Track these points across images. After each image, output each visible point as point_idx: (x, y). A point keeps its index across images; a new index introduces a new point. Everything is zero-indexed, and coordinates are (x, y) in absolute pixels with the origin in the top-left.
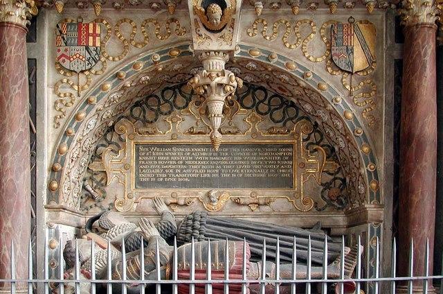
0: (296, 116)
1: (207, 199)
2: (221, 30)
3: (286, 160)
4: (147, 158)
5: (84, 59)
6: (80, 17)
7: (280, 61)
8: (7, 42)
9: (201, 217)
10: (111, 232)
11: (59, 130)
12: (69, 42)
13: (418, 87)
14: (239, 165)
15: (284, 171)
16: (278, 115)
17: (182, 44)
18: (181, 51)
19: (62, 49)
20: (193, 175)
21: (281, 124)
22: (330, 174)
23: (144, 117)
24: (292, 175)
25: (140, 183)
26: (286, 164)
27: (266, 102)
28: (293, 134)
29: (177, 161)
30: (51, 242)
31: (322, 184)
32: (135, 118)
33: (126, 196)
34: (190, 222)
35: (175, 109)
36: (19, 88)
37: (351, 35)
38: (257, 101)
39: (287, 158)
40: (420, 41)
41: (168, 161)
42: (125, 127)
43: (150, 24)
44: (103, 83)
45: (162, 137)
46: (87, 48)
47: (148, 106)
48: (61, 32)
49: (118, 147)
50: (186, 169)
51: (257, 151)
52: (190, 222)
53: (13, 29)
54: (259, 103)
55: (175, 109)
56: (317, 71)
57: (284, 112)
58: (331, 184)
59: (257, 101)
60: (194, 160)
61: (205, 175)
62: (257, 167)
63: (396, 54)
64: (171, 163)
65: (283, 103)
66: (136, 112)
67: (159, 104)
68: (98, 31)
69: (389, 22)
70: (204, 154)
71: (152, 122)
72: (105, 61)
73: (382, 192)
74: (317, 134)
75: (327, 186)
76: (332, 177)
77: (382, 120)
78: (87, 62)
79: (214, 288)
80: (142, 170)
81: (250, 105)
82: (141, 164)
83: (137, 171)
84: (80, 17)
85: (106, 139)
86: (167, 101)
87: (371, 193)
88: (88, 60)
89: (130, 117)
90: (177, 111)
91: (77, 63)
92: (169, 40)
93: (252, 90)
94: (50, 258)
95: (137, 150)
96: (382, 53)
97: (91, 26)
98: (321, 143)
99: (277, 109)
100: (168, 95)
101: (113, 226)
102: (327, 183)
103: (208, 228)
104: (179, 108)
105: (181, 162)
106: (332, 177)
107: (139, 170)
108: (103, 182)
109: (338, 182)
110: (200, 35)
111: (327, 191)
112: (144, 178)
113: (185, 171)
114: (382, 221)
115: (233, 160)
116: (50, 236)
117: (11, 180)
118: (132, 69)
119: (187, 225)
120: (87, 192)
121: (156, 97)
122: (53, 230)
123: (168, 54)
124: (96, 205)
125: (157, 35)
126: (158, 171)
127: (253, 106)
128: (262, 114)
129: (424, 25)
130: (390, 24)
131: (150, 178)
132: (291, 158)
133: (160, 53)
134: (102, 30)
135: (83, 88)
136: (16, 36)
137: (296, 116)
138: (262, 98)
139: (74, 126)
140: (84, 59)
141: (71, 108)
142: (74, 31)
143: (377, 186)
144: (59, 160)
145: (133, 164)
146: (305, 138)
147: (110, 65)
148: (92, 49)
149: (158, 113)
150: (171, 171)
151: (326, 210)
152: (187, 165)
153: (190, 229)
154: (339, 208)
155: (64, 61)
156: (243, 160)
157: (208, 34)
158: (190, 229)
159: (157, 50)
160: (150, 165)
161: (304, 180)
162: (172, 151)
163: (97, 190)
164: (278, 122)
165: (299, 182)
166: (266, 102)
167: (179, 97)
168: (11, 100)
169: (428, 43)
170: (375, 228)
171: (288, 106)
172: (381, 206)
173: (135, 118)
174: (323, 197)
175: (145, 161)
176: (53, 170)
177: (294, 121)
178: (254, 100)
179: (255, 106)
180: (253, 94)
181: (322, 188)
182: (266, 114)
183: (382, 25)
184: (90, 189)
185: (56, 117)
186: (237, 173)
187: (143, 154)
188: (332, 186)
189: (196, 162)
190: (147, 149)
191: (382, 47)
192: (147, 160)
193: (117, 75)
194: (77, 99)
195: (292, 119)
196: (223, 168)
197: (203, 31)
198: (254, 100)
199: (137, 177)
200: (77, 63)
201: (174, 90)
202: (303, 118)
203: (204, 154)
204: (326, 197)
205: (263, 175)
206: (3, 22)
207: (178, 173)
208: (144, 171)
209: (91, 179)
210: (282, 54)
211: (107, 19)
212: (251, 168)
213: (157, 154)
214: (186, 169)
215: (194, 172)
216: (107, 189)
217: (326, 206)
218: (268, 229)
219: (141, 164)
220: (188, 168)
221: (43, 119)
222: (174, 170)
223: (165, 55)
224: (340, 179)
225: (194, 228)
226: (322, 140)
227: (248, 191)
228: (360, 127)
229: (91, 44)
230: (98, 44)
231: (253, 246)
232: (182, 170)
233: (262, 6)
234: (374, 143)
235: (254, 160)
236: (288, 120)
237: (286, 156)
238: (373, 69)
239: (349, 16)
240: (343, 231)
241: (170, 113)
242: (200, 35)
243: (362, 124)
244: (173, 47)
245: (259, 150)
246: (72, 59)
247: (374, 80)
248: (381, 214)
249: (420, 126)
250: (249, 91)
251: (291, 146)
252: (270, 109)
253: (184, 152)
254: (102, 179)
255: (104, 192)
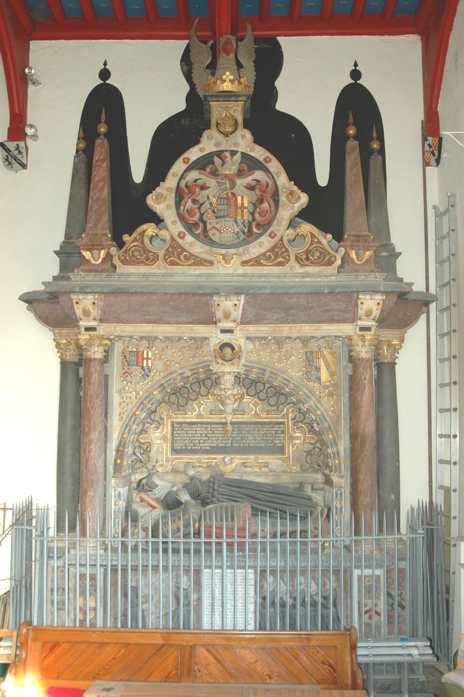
0: (286, 402)
1: (223, 463)
2: (232, 360)
3: (279, 434)
4: (179, 432)
5: (140, 375)
6: (138, 345)
7: (271, 375)
8: (93, 372)
9: (219, 481)
10: (156, 491)
11: (122, 422)
12: (130, 364)
13: (361, 400)
14: (245, 437)
15: (278, 442)
16: (273, 401)
17: (206, 364)
18: (205, 369)
19: (126, 368)
20: (213, 445)
21: (275, 408)
22: (311, 444)
23: (178, 403)
24: (283, 444)
25: (174, 451)
26: (280, 437)
27: (265, 391)
28: (284, 415)
29: (201, 434)
30: (115, 502)
31: (306, 452)
32: (172, 403)
33: (164, 461)
34: (211, 484)
35: (199, 396)
36: (100, 401)
37: (319, 359)
38: (258, 391)
39: (280, 432)
40: (361, 370)
41: (195, 434)
42: (164, 412)
43: (184, 350)
44: (152, 390)
45: (190, 417)
46: (142, 367)
47: (181, 394)
48: (125, 356)
49: (159, 423)
50: (207, 440)
51: (259, 427)
52: (211, 484)
53: (97, 363)
54: (259, 392)
55: (199, 396)
56: (297, 382)
57: (277, 399)
58: (311, 451)
59: (258, 391)
60: (213, 433)
61: (221, 445)
62: (258, 438)
63: (350, 371)
64: (197, 435)
65: (277, 392)
66: (173, 398)
67: (189, 393)
68: (150, 356)
69: (344, 349)
70: (220, 429)
71: (183, 406)
72: (154, 375)
73: (343, 467)
74: (301, 414)
75: (309, 453)
76: (312, 446)
77: (341, 415)
78: (142, 377)
79: (227, 545)
80: (176, 440)
81: (253, 393)
82: (176, 437)
83: (173, 441)
84: (138, 345)
85: (150, 418)
86: (194, 391)
87: (335, 467)
88: (143, 376)
89: (168, 402)
90: (202, 398)
91: (135, 378)
92: (197, 360)
93: (254, 383)
94: (115, 512)
95: (173, 426)
96: (340, 369)
97: (145, 353)
98: (304, 421)
99: (272, 396)
100: (196, 387)
101: (157, 486)
102: (309, 451)
103: (224, 488)
104: (203, 396)
105: (204, 435)
106: (312, 446)
107: (173, 441)
108: (148, 449)
109: (317, 450)
110: (218, 363)
111: (309, 457)
112: (178, 446)
113: (207, 442)
114: (342, 488)
115: (241, 433)
116: (115, 497)
117: (94, 463)
118: (172, 381)
119: (209, 487)
120: (137, 457)
121: (187, 388)
122: (117, 493)
123: (196, 371)
124: (143, 467)
125: (189, 357)
126: (187, 441)
127: (255, 394)
128: (262, 400)
129: (363, 360)
130: (345, 350)
131: (182, 447)
132: (283, 432)
133: (191, 370)
134: (153, 355)
135: (139, 393)
136: (98, 367)
137: (286, 402)
138: (261, 388)
139: (132, 420)
140: (140, 375)
141: (130, 406)
142: (134, 356)
143: (339, 462)
144: (122, 443)
145: (169, 436)
146: (293, 418)
147: (157, 378)
148: (146, 368)
149: (188, 399)
150: (197, 441)
151: (309, 470)
152: (208, 437)
153: (211, 491)
154: (318, 470)
155: (127, 376)
156: (248, 433)
157: (223, 362)
158: (211, 491)
159: (189, 368)
160: (181, 437)
161: (292, 448)
162: (198, 427)
163: (143, 456)
164: (273, 406)
165: (290, 450)
166: (265, 391)
167: (203, 388)
168: (95, 409)
169: (366, 372)
170: (339, 492)
171: (279, 395)
172: (342, 477)
173: (172, 403)
174: (306, 461)
175: (178, 434)
176: (118, 450)
177: (284, 405)
178: (256, 390)
179: (257, 395)
180: (255, 385)
181: (305, 454)
182: (264, 400)
183: (340, 350)
184: (139, 455)
185: (120, 414)
186: (244, 443)
187: (177, 429)
188: (313, 453)
189: (215, 435)
190: (180, 426)
191: (340, 365)
192: (180, 434)
193: (162, 385)
194: (135, 401)
195: (283, 404)
196: (234, 439)
197: (220, 361)
198: (256, 390)
199: (172, 447)
200: (135, 378)
201: (199, 383)
202: (290, 403)
203: (220, 429)
204: (309, 461)
205: (263, 445)
206: (91, 359)
207: (202, 443)
208: (177, 441)
209: (140, 447)
210: (273, 371)
211: (156, 346)
212: (255, 440)
213: (187, 429)
214: (207, 440)
215: (213, 443)
216: (151, 455)
217: (309, 468)
218: (266, 490)
219: (176, 437)
220: (209, 439)
221: (112, 416)
222: (199, 440)
223: (195, 371)
224: (318, 448)
225: (214, 489)
226: (304, 419)
227: (252, 457)
228: (326, 420)
229: (145, 365)
230: (150, 365)
231: (253, 502)
232: (205, 440)
233: (258, 344)
234: (336, 432)
235: (256, 434)
236: (280, 404)
237: (279, 430)
238: (334, 380)
239: (318, 344)
240: (321, 486)
241: (196, 399)
242: (218, 363)
243: (328, 419)
244: (200, 366)
245: (260, 426)
246: (132, 375)
247: (335, 388)
248: (342, 483)
249: (362, 427)
250: (252, 383)
251: (282, 423)
252: (267, 397)
253: (206, 428)
254: (147, 448)
255: (149, 457)
